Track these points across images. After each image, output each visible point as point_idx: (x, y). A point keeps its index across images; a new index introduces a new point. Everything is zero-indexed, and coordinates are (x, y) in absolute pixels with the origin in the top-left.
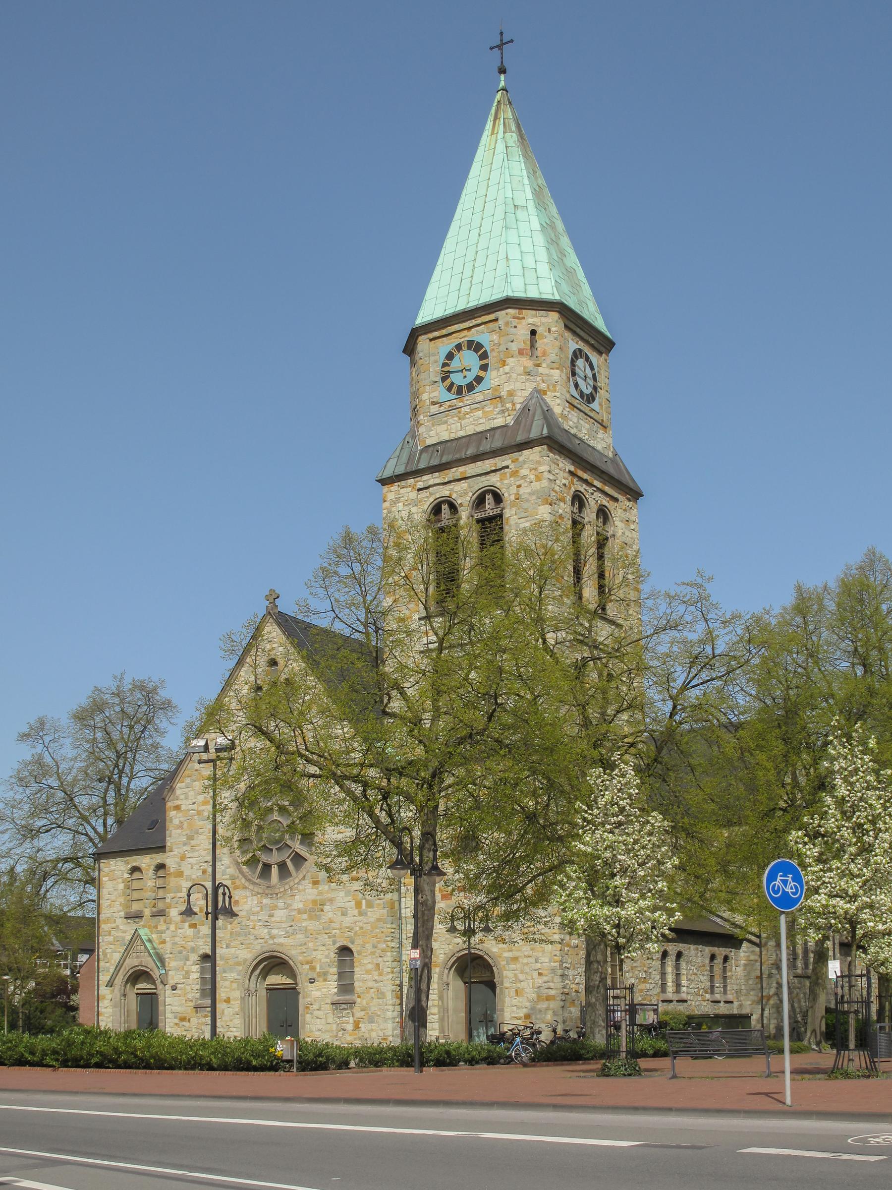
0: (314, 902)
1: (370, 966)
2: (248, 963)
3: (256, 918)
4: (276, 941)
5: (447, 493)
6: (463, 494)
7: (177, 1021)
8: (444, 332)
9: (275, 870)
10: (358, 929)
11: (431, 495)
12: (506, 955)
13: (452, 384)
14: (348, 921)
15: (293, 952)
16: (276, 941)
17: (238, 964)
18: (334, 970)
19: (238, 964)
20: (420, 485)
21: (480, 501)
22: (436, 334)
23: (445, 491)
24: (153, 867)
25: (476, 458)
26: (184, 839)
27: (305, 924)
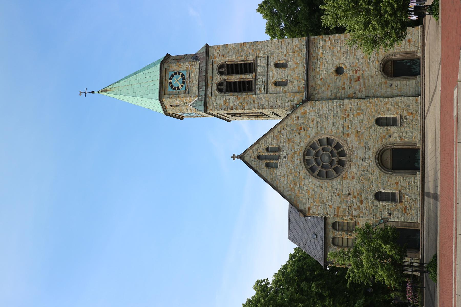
0: (356, 136)
1: (385, 108)
2: (380, 171)
3: (360, 166)
4: (371, 156)
5: (215, 85)
6: (218, 78)
7: (406, 215)
8: (164, 89)
9: (342, 158)
10: (369, 114)
11: (214, 91)
12: (383, 52)
13: (179, 74)
14: (365, 119)
15: (377, 146)
16: (371, 156)
17: (380, 177)
18: (386, 127)
19: (380, 177)
20: (210, 96)
21: (221, 73)
22: (163, 92)
23: (215, 85)
24: (333, 230)
25: (207, 72)
26: (323, 205)
27: (365, 140)
